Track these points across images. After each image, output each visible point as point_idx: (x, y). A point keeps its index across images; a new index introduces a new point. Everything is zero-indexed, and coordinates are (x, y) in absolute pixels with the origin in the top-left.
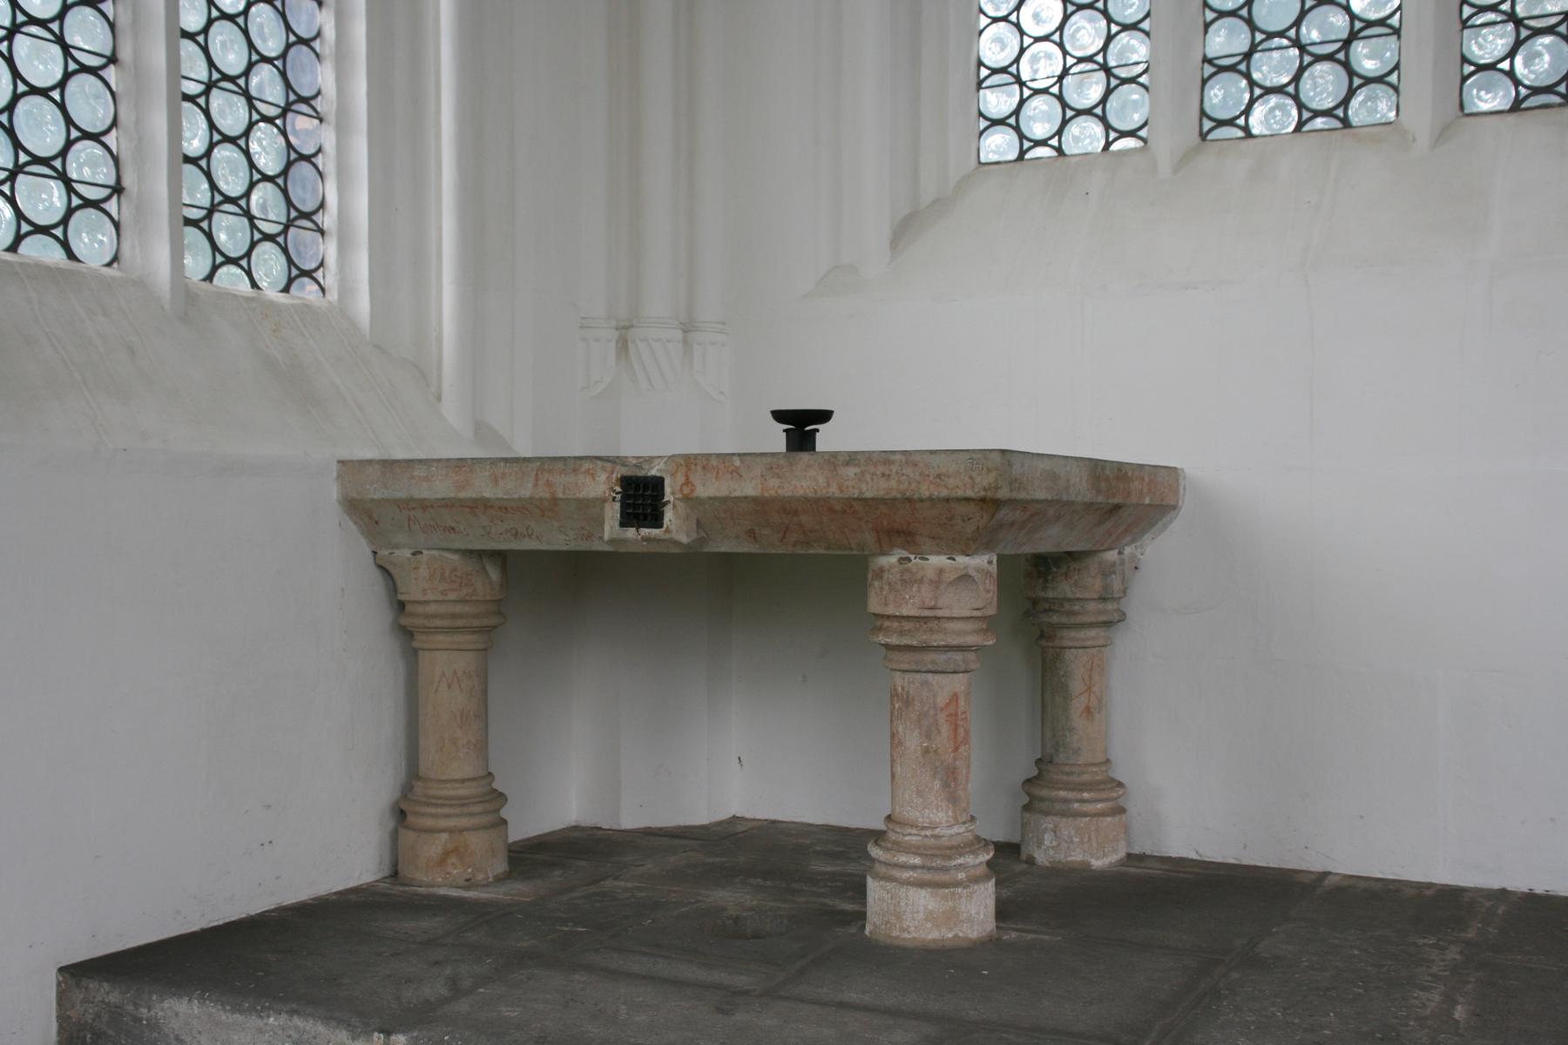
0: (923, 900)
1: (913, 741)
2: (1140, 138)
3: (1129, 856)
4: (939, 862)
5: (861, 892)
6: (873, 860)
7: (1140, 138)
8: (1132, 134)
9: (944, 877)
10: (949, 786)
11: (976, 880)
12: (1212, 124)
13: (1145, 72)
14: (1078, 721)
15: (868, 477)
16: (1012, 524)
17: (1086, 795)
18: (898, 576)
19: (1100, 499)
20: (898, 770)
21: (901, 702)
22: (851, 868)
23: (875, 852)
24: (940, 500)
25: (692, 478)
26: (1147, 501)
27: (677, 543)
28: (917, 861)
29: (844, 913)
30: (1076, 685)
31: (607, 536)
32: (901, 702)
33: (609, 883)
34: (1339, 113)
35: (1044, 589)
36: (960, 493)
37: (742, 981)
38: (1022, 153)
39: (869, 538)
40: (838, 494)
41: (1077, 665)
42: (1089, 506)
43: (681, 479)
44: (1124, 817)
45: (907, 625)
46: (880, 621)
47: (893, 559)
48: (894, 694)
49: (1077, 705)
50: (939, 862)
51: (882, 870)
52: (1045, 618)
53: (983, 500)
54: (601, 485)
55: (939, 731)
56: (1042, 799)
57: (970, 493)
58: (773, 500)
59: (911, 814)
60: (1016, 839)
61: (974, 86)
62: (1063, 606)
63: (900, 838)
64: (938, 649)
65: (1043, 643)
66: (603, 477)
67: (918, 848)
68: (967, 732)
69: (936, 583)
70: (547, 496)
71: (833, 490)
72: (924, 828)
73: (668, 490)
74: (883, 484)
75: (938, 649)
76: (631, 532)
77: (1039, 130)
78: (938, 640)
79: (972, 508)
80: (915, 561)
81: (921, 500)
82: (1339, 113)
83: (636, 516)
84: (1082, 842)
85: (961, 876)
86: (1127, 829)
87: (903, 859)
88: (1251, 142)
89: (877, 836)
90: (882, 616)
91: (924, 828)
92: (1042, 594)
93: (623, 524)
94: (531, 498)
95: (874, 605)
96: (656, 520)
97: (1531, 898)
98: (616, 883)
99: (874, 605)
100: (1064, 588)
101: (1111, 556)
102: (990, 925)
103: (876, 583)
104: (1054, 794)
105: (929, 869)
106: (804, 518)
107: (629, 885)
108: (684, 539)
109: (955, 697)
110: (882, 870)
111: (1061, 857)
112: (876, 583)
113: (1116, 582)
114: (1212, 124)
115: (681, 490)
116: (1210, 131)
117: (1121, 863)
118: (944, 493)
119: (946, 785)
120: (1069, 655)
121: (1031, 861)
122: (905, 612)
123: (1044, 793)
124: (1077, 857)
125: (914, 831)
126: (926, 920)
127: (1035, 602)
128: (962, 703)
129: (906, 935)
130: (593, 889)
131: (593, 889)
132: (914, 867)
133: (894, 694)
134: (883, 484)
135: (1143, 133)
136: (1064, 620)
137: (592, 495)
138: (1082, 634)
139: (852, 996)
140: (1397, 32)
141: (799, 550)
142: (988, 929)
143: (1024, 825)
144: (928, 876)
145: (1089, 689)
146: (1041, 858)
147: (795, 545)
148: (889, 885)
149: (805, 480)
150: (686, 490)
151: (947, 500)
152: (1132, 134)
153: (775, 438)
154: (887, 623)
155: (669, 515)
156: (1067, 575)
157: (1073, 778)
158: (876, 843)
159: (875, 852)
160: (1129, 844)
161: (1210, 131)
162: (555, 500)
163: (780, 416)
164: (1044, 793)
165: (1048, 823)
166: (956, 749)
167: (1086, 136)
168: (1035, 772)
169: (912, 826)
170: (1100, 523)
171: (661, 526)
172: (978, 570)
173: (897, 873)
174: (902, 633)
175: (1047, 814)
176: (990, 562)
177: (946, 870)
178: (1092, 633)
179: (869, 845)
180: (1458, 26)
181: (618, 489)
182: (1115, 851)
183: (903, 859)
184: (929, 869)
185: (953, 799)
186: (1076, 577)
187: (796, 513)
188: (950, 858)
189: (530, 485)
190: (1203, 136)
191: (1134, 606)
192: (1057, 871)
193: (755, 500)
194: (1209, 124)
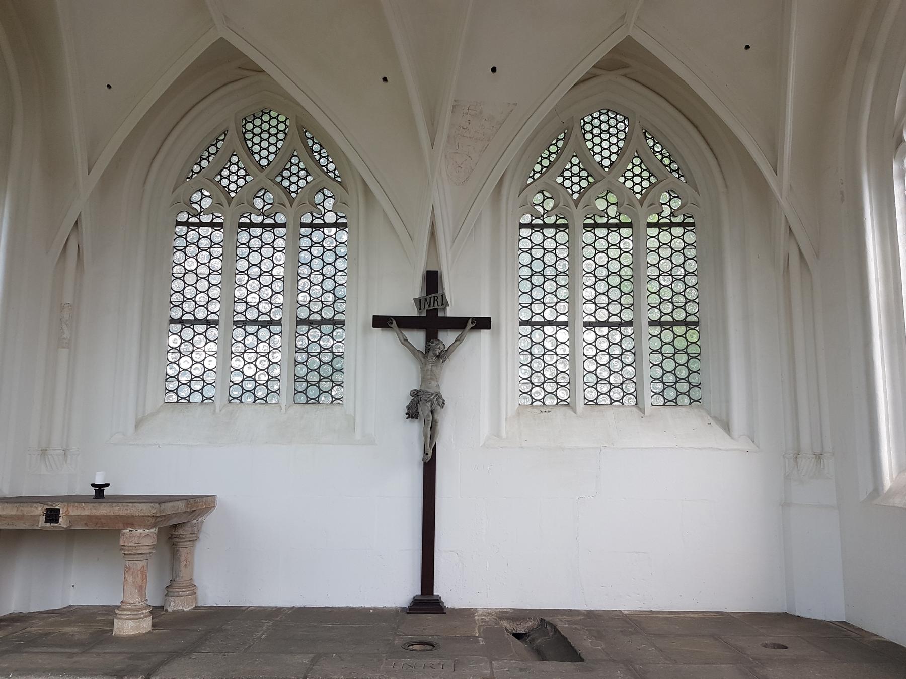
0: (131, 623)
1: (130, 580)
2: (212, 400)
3: (196, 606)
4: (135, 613)
5: (112, 623)
6: (116, 614)
7: (212, 400)
8: (210, 399)
9: (137, 617)
10: (140, 591)
11: (146, 617)
12: (232, 398)
13: (214, 382)
14: (183, 568)
15: (122, 510)
16: (161, 520)
17: (184, 590)
18: (129, 535)
19: (189, 510)
20: (125, 588)
21: (127, 569)
22: (110, 617)
23: (117, 611)
24: (141, 516)
25: (69, 509)
26: (204, 507)
27: (63, 527)
28: (129, 613)
29: (107, 630)
30: (183, 558)
31: (40, 526)
32: (127, 569)
33: (28, 629)
34: (265, 399)
35: (174, 531)
36: (147, 514)
37: (76, 650)
38: (178, 400)
39: (121, 525)
40: (113, 514)
41: (183, 552)
42: (185, 512)
43: (65, 509)
44: (195, 595)
45: (131, 548)
46: (122, 548)
47: (128, 530)
48: (126, 567)
49: (183, 564)
50: (135, 613)
51: (119, 616)
52: (174, 540)
53: (153, 516)
54: (39, 510)
55: (138, 577)
56: (171, 592)
57: (150, 515)
58: (93, 516)
59: (128, 600)
60: (163, 605)
61: (165, 380)
62: (179, 536)
63: (125, 607)
64: (139, 554)
65: (174, 546)
66: (40, 509)
67: (130, 609)
68: (146, 576)
69: (139, 537)
70: (21, 514)
71: (112, 513)
72: (132, 604)
73: (61, 512)
74: (126, 512)
75: (139, 554)
76: (48, 524)
77: (183, 395)
78: (138, 552)
79: (150, 518)
80: (134, 531)
81: (136, 516)
82: (265, 399)
83: (50, 520)
84: (182, 604)
85: (142, 616)
86: (196, 599)
87: (125, 613)
88: (242, 405)
89: (118, 607)
90: (123, 546)
91: (132, 604)
92: (174, 533)
93: (45, 522)
94: (15, 515)
95: (121, 543)
96: (57, 521)
97: (300, 607)
98: (31, 629)
99: (121, 543)
100: (181, 531)
101: (195, 521)
102: (150, 629)
103: (122, 537)
104: (174, 590)
105: (133, 615)
106: (102, 520)
107: (36, 629)
108: (65, 526)
109: (143, 567)
110: (119, 616)
111: (175, 609)
112: (122, 537)
113: (196, 529)
114: (232, 398)
115: (65, 513)
116: (231, 400)
117: (193, 609)
118: (143, 514)
119: (139, 591)
120: (181, 550)
121: (166, 610)
122: (130, 545)
123: (171, 590)
124: (180, 608)
125: (129, 605)
126: (131, 629)
127: (172, 535)
128: (145, 568)
129: (125, 634)
130: (23, 631)
131: (23, 631)
132: (128, 615)
133: (126, 567)
134: (126, 512)
135: (213, 399)
136: (180, 540)
137: (36, 514)
138: (185, 544)
139: (108, 651)
140: (279, 380)
141: (100, 528)
142: (149, 630)
143: (165, 600)
144: (132, 617)
145: (187, 559)
146: (170, 610)
147: (99, 527)
148: (121, 620)
149: (103, 510)
150: (67, 513)
151: (143, 516)
152: (210, 399)
153: (92, 491)
154: (125, 548)
155: (61, 519)
156: (181, 527)
157: (181, 585)
158: (118, 609)
159: (117, 611)
160: (196, 603)
161: (231, 400)
162: (23, 515)
163: (93, 485)
164: (171, 590)
165: (172, 599)
166: (143, 581)
167: (280, 145)
168: (170, 584)
169: (128, 603)
170: (189, 515)
171: (58, 523)
172: (151, 533)
173: (123, 617)
174: (129, 551)
175: (172, 596)
176: (155, 530)
177: (137, 614)
178: (188, 543)
179: (116, 610)
180: (294, 381)
181: (45, 512)
182: (192, 606)
183: (125, 613)
184: (133, 615)
185: (141, 595)
186: (184, 528)
187: (100, 519)
188: (139, 611)
189: (15, 511)
190: (229, 401)
191: (201, 536)
192: (174, 612)
193: (88, 515)
194: (231, 399)
